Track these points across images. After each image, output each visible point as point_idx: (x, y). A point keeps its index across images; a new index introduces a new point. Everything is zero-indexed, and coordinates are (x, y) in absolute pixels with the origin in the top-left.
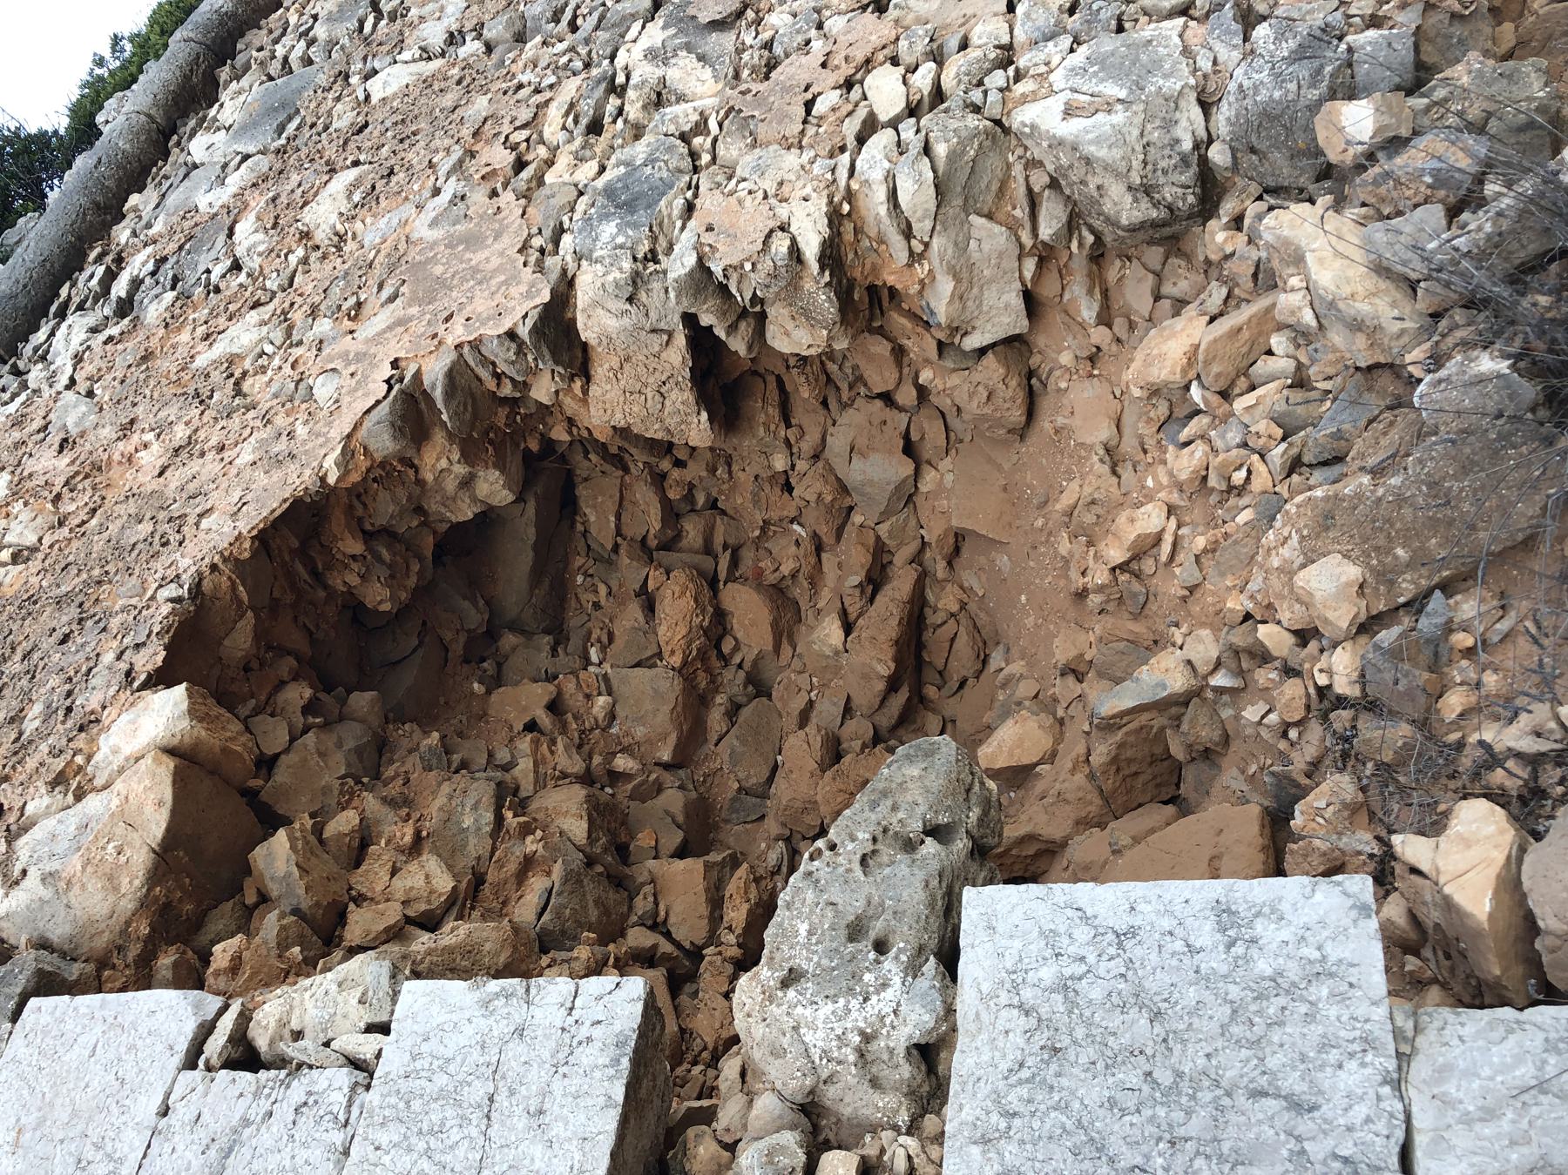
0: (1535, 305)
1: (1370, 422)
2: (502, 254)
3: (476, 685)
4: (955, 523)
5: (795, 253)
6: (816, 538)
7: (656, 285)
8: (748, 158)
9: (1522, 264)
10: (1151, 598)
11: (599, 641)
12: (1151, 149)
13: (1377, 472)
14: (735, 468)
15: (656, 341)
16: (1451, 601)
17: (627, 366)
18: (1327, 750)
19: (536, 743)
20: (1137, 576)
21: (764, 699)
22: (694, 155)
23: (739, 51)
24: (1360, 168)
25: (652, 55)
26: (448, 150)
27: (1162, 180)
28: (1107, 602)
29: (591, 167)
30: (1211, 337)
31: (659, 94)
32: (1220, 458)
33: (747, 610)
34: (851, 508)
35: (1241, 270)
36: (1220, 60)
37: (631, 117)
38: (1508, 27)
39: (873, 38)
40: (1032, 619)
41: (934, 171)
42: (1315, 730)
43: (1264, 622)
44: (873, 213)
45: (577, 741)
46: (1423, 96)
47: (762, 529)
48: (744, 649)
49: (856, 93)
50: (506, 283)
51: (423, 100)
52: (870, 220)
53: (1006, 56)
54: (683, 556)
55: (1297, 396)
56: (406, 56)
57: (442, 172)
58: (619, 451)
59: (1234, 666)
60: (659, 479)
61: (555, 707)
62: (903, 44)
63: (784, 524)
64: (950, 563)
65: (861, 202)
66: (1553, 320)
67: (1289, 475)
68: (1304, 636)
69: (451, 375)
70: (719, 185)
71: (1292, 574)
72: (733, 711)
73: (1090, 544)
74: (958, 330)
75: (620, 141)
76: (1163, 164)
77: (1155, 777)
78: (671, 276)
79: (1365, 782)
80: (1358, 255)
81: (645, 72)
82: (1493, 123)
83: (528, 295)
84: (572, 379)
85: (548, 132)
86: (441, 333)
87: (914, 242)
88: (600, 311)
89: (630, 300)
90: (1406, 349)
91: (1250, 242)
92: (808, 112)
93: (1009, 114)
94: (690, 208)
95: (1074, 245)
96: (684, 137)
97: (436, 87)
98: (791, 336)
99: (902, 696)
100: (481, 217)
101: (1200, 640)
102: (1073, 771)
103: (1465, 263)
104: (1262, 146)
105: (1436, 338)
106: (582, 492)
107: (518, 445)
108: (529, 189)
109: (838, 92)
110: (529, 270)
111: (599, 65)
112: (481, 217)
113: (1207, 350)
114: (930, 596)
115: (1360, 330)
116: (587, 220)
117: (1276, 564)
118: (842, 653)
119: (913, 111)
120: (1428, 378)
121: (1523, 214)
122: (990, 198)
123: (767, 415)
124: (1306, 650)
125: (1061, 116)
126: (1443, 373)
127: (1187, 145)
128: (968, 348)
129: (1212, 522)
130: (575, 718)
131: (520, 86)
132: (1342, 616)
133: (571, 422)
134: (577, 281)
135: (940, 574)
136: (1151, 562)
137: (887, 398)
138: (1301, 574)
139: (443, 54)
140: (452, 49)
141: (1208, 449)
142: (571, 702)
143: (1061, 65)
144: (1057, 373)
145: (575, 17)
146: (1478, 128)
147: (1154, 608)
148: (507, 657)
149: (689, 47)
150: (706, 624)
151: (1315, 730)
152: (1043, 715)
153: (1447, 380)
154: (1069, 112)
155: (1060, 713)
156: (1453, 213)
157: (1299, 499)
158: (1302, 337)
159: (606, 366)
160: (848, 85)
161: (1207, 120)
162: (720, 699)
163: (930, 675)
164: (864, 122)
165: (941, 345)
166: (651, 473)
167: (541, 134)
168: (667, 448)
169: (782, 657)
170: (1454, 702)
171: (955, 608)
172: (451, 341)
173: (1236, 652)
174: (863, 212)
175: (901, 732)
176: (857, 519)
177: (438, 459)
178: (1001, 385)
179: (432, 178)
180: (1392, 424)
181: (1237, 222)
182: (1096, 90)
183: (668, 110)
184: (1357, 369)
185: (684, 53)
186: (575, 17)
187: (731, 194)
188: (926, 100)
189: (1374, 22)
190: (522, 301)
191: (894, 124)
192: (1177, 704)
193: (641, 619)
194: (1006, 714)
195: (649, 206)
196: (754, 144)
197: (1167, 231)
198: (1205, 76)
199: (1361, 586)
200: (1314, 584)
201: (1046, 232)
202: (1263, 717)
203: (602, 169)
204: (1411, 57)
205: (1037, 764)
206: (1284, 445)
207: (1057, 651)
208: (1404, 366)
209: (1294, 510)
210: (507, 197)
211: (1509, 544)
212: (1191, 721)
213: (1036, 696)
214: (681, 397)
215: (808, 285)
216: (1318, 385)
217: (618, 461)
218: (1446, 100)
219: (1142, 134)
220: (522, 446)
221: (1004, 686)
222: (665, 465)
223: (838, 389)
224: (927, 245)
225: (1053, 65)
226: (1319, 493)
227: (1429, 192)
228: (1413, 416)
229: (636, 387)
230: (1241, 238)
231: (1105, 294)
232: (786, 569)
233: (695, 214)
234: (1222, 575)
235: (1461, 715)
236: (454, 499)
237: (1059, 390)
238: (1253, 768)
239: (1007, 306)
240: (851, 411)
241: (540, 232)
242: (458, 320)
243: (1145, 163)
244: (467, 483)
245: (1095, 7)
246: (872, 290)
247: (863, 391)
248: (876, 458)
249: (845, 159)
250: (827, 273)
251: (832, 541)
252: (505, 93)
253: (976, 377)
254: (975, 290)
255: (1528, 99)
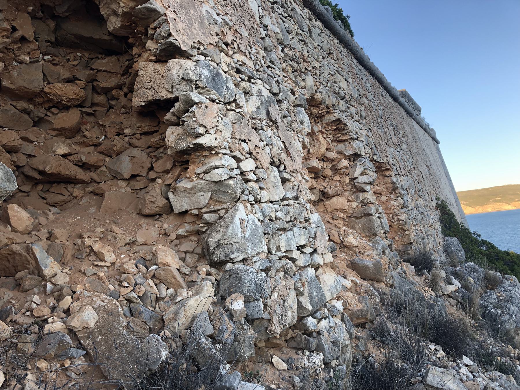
0: (183, 364)
1: (145, 323)
2: (198, 34)
3: (31, 8)
4: (107, 193)
5: (199, 135)
6: (100, 144)
7: (188, 88)
8: (229, 121)
9: (196, 359)
10: (81, 260)
11: (54, 60)
12: (231, 246)
13: (128, 327)
14: (125, 115)
15: (169, 87)
16: (82, 357)
17: (160, 76)
18: (22, 326)
19: (7, 30)
20: (89, 255)
21: (32, 124)
22: (229, 103)
23: (260, 119)
24: (224, 307)
25: (260, 91)
26: (231, 20)
27: (221, 250)
28: (79, 246)
29: (226, 69)
30: (172, 270)
31: (248, 93)
32: (131, 277)
33: (70, 119)
34: (111, 157)
35: (194, 277)
36: (256, 263)
37: (241, 84)
38: (264, 344)
39: (264, 161)
40: (71, 221)
41: (225, 180)
42: (30, 321)
43: (72, 298)
44: (212, 161)
45: (9, 47)
46: (245, 322)
47: (102, 125)
48: (53, 117)
49: (248, 156)
50: (188, 35)
51: (247, 14)
52: (209, 160)
53: (258, 201)
54: (90, 96)
55: (154, 299)
56: (261, 11)
57: (224, 17)
58: (130, 73)
59: (55, 290)
60: (120, 87)
61: (23, 39)
62: (262, 170)
63: (104, 133)
64: (92, 192)
65: (215, 157)
66: (178, 370)
67: (126, 300)
68: (68, 312)
69: (155, 11)
70: (220, 111)
71: (91, 305)
72: (27, 112)
73: (100, 238)
74: (175, 191)
75: (234, 79)
76: (226, 250)
77: (8, 268)
78: (191, 93)
79: (9, 340)
80: (199, 311)
81: (255, 89)
82: (237, 343)
83: (184, 42)
84: (155, 56)
85: (237, 55)
86: (170, 9)
87: (203, 174)
88: (179, 67)
89: (183, 78)
90: (169, 330)
91: (203, 279)
92: (242, 141)
93: (241, 202)
94: (213, 101)
95: (202, 225)
96: (235, 101)
97: (251, 19)
98: (172, 135)
99: (38, 177)
100: (210, 29)
101: (64, 278)
102: (8, 238)
103: (196, 342)
104: (231, 279)
105: (172, 338)
106: (114, 58)
107: (130, 35)
108: (219, 47)
109: (248, 150)
110: (192, 43)
111: (257, 74)
112: (210, 29)
113: (168, 269)
114: (78, 186)
115: (175, 315)
116: (209, 66)
117: (94, 299)
118: (55, 154)
119: (242, 173)
120: (159, 337)
121: (210, 356)
122: (216, 198)
123: (145, 127)
124: (62, 313)
125: (240, 218)
126: (161, 341)
127: (232, 256)
128: (169, 194)
129: (109, 277)
130: (19, 47)
131: (251, 48)
132: (75, 323)
133: (140, 55)
134: (189, 60)
135: (87, 189)
136: (94, 259)
137: (151, 169)
138: (91, 308)
139: (261, 23)
140: (263, 26)
141: (135, 273)
142: (26, 46)
143: (256, 217)
144: (161, 223)
145: (271, 68)
146: (235, 339)
147: (77, 262)
148: (44, 22)
149: (262, 103)
150: (63, 102)
151: (30, 321)
152: (32, 227)
153: (159, 343)
154: (242, 220)
155: (33, 233)
156: (211, 336)
157: (118, 304)
158: (173, 298)
159: (160, 69)
160: (250, 153)
161: (239, 262)
162: (31, 107)
163: (47, 187)
164: (239, 158)
165: (169, 185)
166: (122, 85)
167: (236, 53)
168: (131, 90)
169: (51, 131)
170: (43, 365)
171: (74, 195)
172: (167, 12)
173: (60, 290)
174: (212, 158)
175: (22, 176)
176: (107, 159)
177: (123, 2)
178: (156, 205)
179: (222, 14)
180: (144, 329)
181: (209, 274)
182: (248, 228)
183: (243, 95)
184: (163, 316)
185: (260, 102)
186: (271, 68)
187: (217, 115)
188: (246, 177)
189: (265, 306)
190: (182, 40)
191: (239, 167)
192: (39, 273)
193: (63, 77)
194: (30, 213)
195: (213, 87)
196: (233, 123)
197: (206, 253)
198: (251, 260)
199: (87, 328)
200: (87, 312)
201: (206, 216)
202: (35, 302)
203: (225, 72)
204: (256, 317)
205: (11, 226)
206: (136, 296)
207: (58, 230)
208: (163, 330)
209: (114, 302)
210: (217, 39)
211: (103, 371)
212: (32, 278)
213: (40, 224)
214: (150, 96)
215: (189, 140)
216: (157, 305)
217: (126, 73)
218: (243, 329)
219: (235, 242)
220: (130, 36)
221: (43, 212)
222: (125, 90)
223: (154, 152)
224: (202, 179)
225: (255, 215)
226: (120, 309)
227: (217, 328)
228: (147, 335)
229: (153, 79)
230: (204, 276)
231: (187, 236)
232: (87, 133)
233: (211, 103)
234: (90, 283)
235: (38, 367)
236: (108, 7)
237: (155, 224)
238: (13, 302)
239: (182, 205)
240: (147, 156)
241: (205, 49)
242: (175, 16)
243: (227, 244)
244: (115, 13)
245: (271, 226)
246: (187, 162)
247: (154, 160)
248: (130, 165)
249: (228, 152)
250: (193, 146)
251: (98, 150)
252: (249, 42)
253: (159, 197)
254: (188, 195)
255: (244, 352)
